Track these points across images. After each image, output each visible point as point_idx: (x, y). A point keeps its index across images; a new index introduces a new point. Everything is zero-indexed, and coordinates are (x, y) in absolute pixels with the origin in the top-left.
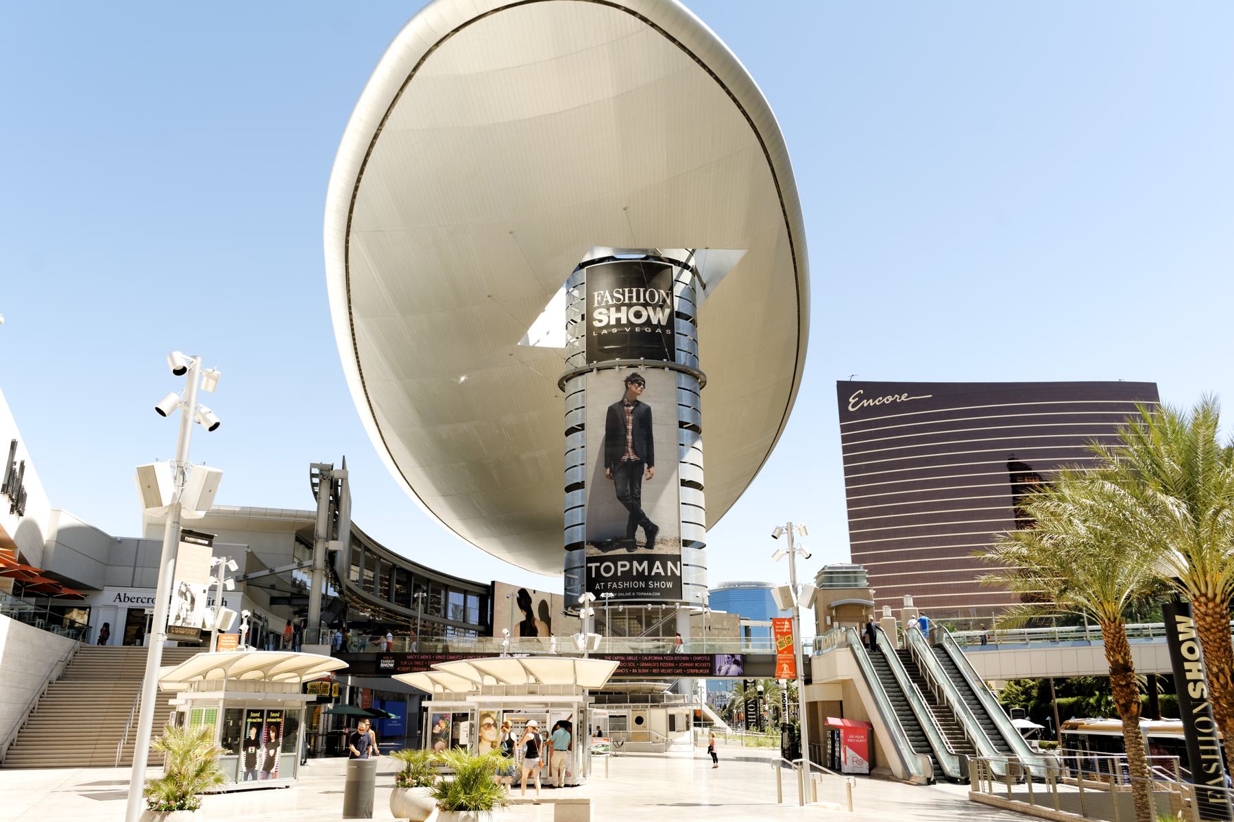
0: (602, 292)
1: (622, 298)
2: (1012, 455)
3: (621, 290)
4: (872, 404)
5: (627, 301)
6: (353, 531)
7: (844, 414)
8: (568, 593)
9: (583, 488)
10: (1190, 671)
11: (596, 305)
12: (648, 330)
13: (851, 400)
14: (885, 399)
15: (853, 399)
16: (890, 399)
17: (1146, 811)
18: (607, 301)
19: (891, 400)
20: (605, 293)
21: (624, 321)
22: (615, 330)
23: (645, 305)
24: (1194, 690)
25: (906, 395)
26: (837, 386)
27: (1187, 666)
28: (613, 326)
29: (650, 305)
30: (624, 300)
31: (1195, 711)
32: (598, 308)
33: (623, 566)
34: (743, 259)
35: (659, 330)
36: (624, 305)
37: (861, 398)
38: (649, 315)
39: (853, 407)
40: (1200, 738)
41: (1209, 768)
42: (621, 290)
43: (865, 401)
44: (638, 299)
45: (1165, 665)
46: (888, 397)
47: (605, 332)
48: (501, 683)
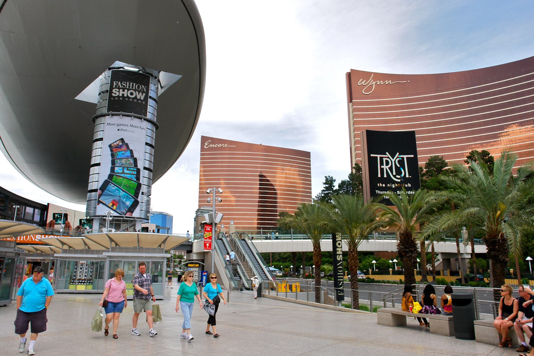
0: (117, 82)
1: (126, 86)
2: (261, 172)
3: (125, 83)
5: (128, 87)
7: (202, 149)
8: (88, 211)
9: (100, 166)
10: (338, 251)
11: (114, 87)
12: (135, 101)
13: (206, 144)
18: (119, 86)
20: (118, 82)
21: (125, 95)
22: (121, 99)
23: (135, 90)
24: (116, 91)
26: (201, 138)
27: (338, 249)
28: (121, 97)
29: (137, 91)
30: (127, 87)
31: (338, 265)
32: (114, 88)
34: (181, 77)
35: (131, 100)
36: (126, 89)
37: (210, 143)
38: (136, 95)
39: (206, 147)
40: (338, 274)
41: (340, 283)
42: (125, 83)
44: (133, 87)
45: (330, 249)
47: (117, 98)
48: (71, 249)
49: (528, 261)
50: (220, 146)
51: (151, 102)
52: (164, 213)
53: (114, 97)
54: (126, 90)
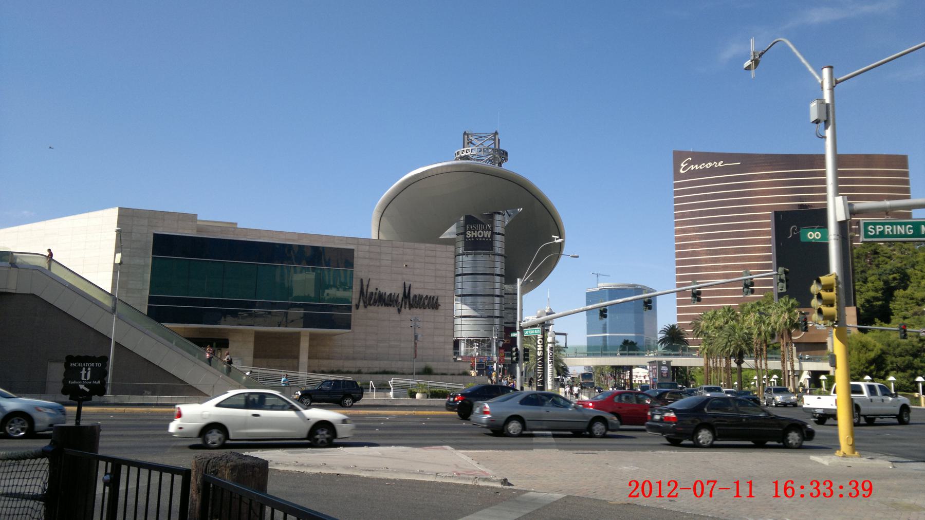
4: (697, 168)
6: (493, 429)
12: (484, 239)
14: (707, 165)
15: (684, 164)
16: (710, 164)
17: (362, 304)
19: (710, 165)
21: (476, 236)
22: (473, 239)
25: (722, 162)
33: (879, 228)
35: (480, 239)
37: (690, 163)
43: (693, 166)
46: (709, 163)
49: (918, 382)
50: (708, 166)
51: (498, 237)
52: (638, 285)
53: (468, 239)
54: (476, 231)
